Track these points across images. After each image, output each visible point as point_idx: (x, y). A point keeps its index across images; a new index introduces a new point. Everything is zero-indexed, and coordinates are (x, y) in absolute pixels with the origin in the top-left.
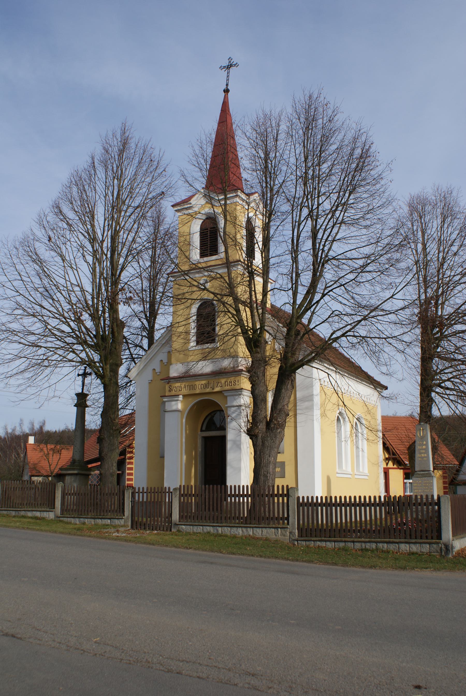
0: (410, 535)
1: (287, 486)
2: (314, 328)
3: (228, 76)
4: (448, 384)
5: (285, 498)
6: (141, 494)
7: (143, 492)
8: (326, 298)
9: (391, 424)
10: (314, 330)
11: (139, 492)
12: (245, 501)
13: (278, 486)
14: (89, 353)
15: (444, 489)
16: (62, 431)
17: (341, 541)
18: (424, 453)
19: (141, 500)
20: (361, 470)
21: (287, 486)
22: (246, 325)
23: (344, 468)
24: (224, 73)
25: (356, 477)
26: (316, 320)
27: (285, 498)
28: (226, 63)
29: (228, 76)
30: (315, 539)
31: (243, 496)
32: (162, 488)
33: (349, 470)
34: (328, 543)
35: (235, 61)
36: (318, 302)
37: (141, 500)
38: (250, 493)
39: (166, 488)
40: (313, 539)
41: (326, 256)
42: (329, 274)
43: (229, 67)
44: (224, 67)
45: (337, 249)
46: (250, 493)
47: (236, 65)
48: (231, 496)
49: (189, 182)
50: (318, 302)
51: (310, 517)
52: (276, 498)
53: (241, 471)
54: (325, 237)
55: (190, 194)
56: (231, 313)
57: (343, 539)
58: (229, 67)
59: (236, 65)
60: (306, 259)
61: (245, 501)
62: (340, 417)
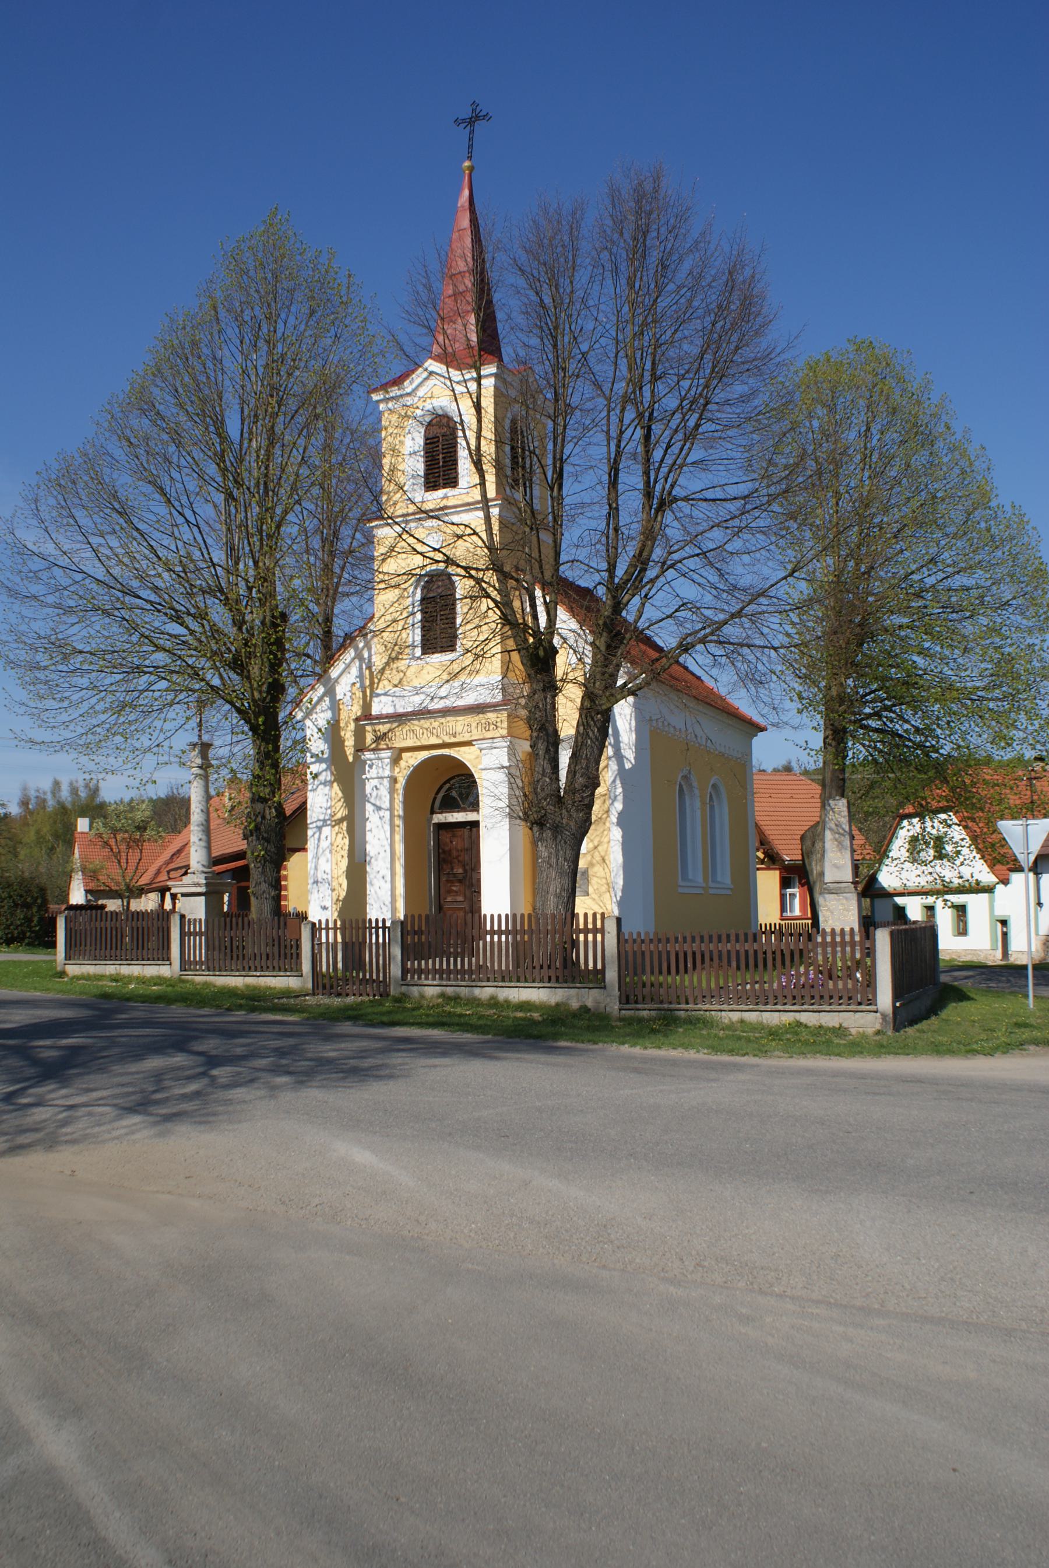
1: (603, 914)
2: (648, 628)
3: (471, 139)
4: (873, 723)
5: (599, 936)
7: (327, 929)
8: (671, 573)
10: (647, 632)
11: (321, 929)
14: (225, 676)
15: (476, 824)
19: (591, 966)
20: (719, 879)
21: (603, 914)
22: (521, 621)
24: (463, 133)
25: (712, 891)
26: (651, 613)
27: (599, 936)
28: (467, 113)
29: (471, 139)
31: (500, 932)
32: (364, 921)
33: (700, 879)
35: (484, 108)
36: (652, 581)
37: (591, 966)
39: (370, 920)
41: (670, 493)
42: (672, 527)
43: (472, 121)
44: (464, 121)
45: (689, 483)
47: (487, 117)
48: (492, 932)
49: (405, 348)
50: (652, 581)
54: (669, 460)
55: (403, 369)
56: (493, 600)
58: (472, 121)
59: (487, 117)
60: (631, 503)
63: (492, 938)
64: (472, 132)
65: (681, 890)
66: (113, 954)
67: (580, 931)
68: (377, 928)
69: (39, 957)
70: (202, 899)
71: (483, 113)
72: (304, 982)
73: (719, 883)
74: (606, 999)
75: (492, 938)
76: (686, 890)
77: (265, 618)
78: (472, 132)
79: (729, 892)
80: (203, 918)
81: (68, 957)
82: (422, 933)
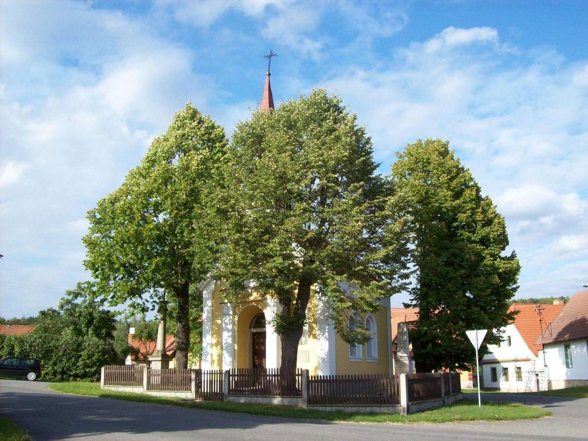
0: (313, 402)
1: (301, 369)
3: (269, 63)
6: (213, 375)
9: (575, 312)
11: (215, 374)
12: (274, 379)
13: (298, 369)
16: (580, 320)
17: (337, 406)
18: (403, 344)
21: (301, 369)
23: (357, 354)
29: (269, 63)
30: (319, 405)
33: (361, 356)
34: (361, 408)
38: (279, 373)
40: (318, 405)
46: (279, 373)
51: (320, 388)
52: (268, 377)
53: (272, 361)
56: (475, 242)
57: (338, 405)
59: (276, 55)
61: (274, 379)
62: (370, 319)
63: (269, 378)
64: (270, 61)
65: (350, 360)
66: (169, 388)
67: (297, 375)
68: (212, 374)
69: (474, 407)
70: (161, 362)
71: (274, 53)
72: (144, 391)
73: (373, 357)
74: (302, 404)
75: (269, 378)
76: (369, 361)
77: (500, 248)
78: (270, 61)
79: (377, 361)
80: (160, 369)
81: (105, 384)
82: (246, 376)
